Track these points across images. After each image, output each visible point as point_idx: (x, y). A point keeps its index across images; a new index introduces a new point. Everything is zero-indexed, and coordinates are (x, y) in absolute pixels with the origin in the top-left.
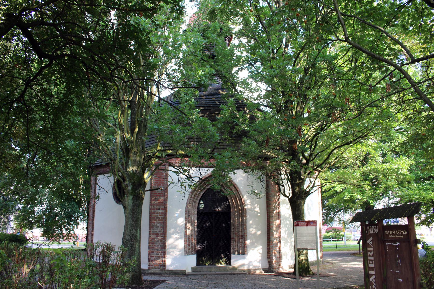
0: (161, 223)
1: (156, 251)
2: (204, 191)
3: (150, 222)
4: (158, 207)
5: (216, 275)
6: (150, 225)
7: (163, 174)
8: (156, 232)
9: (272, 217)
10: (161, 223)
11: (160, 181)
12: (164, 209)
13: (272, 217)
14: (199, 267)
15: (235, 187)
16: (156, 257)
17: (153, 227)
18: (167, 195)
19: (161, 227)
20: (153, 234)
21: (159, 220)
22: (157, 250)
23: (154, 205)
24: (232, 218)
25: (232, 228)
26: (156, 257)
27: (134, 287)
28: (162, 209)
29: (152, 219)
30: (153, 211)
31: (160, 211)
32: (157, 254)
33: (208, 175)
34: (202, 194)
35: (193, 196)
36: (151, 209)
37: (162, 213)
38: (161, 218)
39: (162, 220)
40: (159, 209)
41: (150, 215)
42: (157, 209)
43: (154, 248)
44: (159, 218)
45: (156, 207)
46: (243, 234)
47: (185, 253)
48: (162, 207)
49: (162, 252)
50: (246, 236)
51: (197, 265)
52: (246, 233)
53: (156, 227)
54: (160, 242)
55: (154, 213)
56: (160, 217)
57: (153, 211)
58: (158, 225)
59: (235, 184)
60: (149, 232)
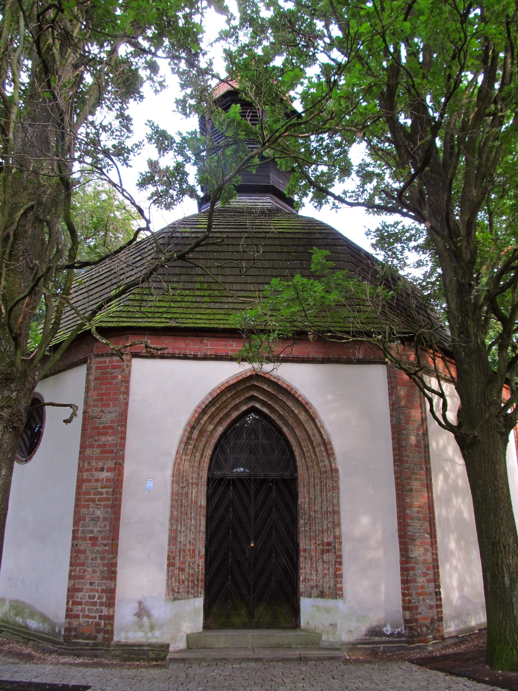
0: (105, 506)
1: (88, 586)
2: (225, 424)
3: (77, 506)
4: (100, 464)
5: (252, 664)
6: (76, 513)
7: (116, 377)
8: (92, 531)
9: (411, 490)
10: (105, 506)
11: (109, 394)
12: (114, 469)
13: (411, 490)
14: (210, 633)
15: (307, 411)
16: (87, 603)
17: (84, 519)
18: (124, 433)
19: (105, 519)
20: (84, 539)
21: (100, 500)
22: (91, 584)
23: (90, 458)
24: (300, 495)
25: (301, 522)
26: (87, 603)
27: (512, 580)
28: (109, 470)
29: (83, 497)
30: (85, 475)
31: (104, 475)
32: (90, 597)
33: (235, 380)
34: (220, 430)
35: (196, 433)
36: (81, 470)
37: (108, 480)
38: (107, 493)
39: (107, 499)
40: (102, 470)
41: (79, 487)
42: (96, 470)
43: (83, 577)
44: (101, 494)
45: (94, 464)
46: (331, 539)
47: (168, 594)
48: (110, 464)
49: (103, 591)
50: (340, 543)
51: (206, 627)
52: (340, 537)
53: (92, 519)
54: (99, 561)
55: (89, 481)
56: (104, 490)
57: (85, 475)
58: (98, 513)
59: (307, 403)
60: (74, 531)
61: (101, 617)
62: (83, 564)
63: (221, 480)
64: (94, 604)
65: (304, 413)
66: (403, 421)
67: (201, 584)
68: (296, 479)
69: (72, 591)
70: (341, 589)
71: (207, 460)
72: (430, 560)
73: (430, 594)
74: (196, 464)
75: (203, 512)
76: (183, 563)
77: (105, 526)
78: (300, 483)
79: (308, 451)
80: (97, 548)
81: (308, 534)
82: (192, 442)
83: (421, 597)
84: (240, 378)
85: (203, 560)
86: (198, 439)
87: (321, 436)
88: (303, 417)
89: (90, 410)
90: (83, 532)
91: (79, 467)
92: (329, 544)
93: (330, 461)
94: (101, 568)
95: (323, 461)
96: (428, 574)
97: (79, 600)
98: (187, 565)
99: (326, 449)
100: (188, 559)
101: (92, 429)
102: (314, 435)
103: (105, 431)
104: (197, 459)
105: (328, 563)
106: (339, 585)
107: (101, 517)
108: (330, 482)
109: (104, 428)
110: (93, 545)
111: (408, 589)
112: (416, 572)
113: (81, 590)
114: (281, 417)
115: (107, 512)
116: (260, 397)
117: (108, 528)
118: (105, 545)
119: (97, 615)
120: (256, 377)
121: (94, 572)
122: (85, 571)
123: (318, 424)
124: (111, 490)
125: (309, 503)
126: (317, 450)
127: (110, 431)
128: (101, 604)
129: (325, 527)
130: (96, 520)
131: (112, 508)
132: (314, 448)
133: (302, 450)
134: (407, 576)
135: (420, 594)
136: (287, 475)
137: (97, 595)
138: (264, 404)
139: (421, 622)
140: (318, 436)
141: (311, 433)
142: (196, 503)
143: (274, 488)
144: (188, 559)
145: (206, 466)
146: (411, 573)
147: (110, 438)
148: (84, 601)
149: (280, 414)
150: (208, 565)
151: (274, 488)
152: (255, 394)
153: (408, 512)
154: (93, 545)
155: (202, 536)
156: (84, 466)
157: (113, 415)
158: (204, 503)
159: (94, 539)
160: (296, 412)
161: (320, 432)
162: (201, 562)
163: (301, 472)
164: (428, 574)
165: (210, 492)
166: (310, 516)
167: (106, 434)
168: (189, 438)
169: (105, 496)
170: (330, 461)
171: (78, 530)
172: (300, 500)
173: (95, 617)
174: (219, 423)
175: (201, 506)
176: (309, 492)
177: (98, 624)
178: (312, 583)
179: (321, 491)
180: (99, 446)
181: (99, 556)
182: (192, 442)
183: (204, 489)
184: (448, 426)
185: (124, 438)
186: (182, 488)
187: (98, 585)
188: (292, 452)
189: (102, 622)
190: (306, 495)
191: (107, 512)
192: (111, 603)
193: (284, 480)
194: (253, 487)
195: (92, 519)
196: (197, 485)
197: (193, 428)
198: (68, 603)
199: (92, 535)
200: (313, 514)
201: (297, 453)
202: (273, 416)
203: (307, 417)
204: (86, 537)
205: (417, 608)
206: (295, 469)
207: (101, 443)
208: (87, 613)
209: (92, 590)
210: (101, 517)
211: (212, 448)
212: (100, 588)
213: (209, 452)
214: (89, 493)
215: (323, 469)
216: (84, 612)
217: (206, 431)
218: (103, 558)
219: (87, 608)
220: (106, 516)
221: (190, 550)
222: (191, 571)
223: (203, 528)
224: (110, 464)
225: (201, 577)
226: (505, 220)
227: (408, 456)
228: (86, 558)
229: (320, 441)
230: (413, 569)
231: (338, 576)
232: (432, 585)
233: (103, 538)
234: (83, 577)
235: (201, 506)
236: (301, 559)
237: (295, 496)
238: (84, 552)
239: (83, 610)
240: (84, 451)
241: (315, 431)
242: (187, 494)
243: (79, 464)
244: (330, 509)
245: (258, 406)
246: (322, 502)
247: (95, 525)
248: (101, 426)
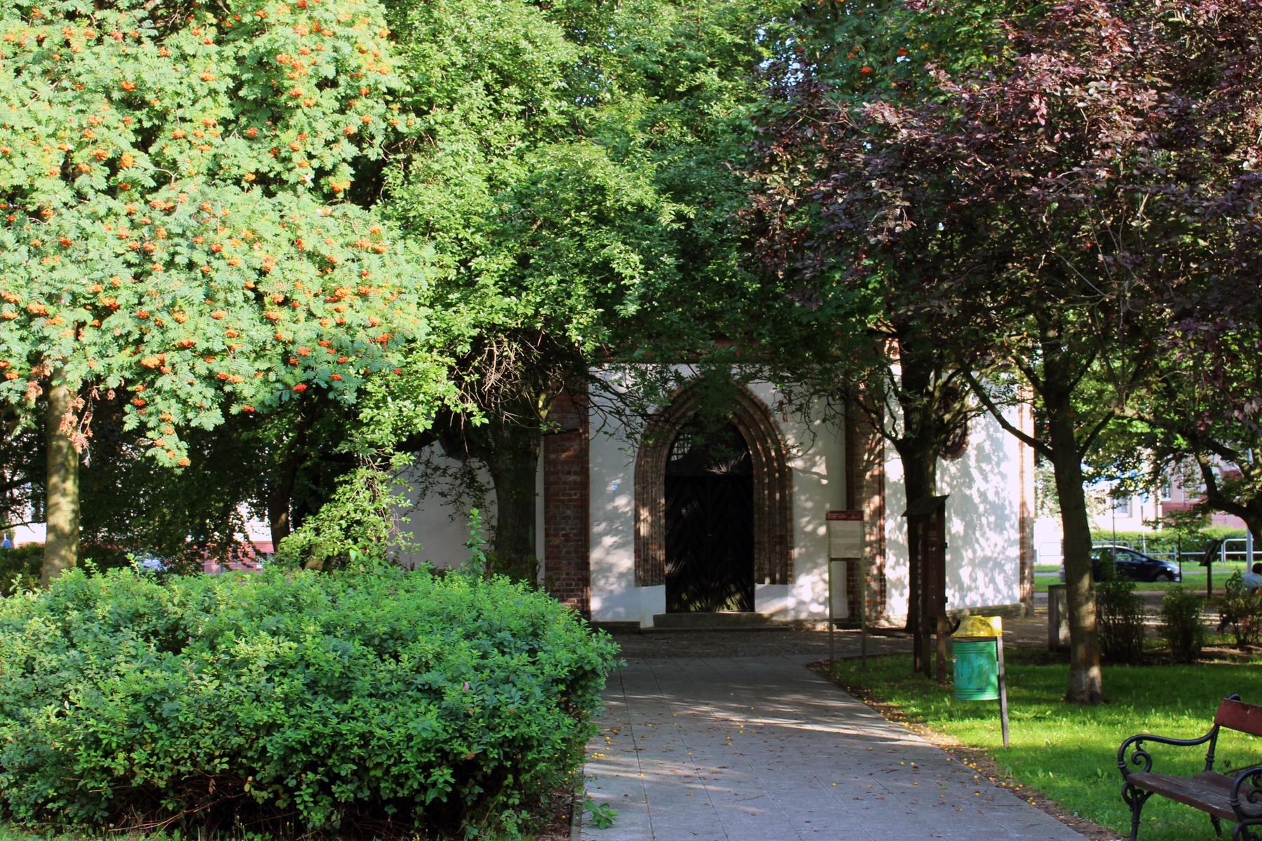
20: (556, 535)
28: (576, 473)
31: (572, 478)
37: (575, 482)
40: (569, 473)
53: (564, 518)
58: (569, 512)
88: (758, 416)
195: (564, 518)
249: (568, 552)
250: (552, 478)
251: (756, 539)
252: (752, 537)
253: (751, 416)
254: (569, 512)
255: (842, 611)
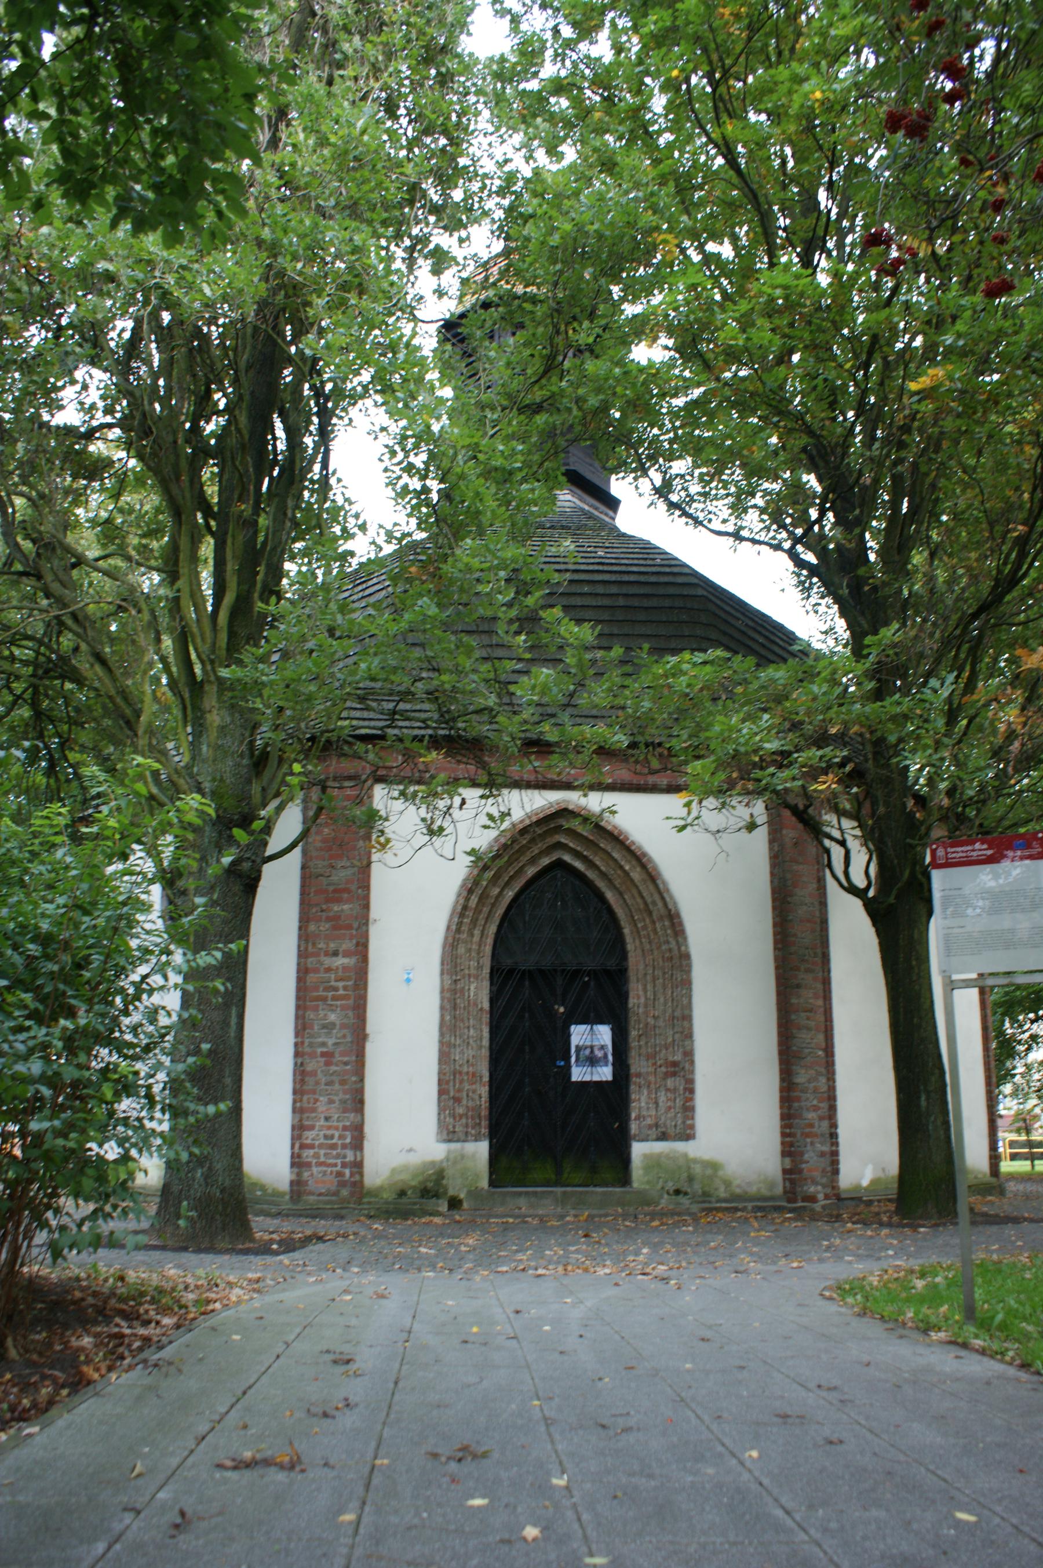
1: (322, 1122)
2: (517, 885)
8: (324, 1044)
10: (343, 1008)
15: (644, 866)
18: (366, 898)
19: (343, 1026)
20: (312, 1055)
21: (334, 998)
22: (327, 1119)
24: (631, 994)
25: (633, 1033)
26: (321, 1146)
28: (347, 954)
31: (340, 961)
34: (510, 894)
35: (474, 900)
37: (345, 968)
38: (345, 988)
40: (335, 954)
42: (327, 954)
44: (336, 989)
45: (322, 945)
46: (678, 1057)
53: (324, 1027)
54: (337, 1086)
55: (316, 971)
56: (340, 984)
58: (332, 1017)
59: (644, 854)
61: (344, 1165)
62: (314, 1092)
63: (511, 972)
64: (333, 1147)
65: (638, 869)
66: (789, 883)
67: (485, 1123)
68: (626, 970)
69: (298, 1130)
70: (692, 1127)
71: (490, 941)
72: (825, 1088)
73: (822, 1135)
74: (474, 947)
75: (486, 1018)
76: (459, 1091)
77: (344, 1036)
78: (632, 974)
79: (645, 928)
80: (333, 1068)
81: (643, 1051)
82: (470, 913)
83: (808, 1140)
84: (541, 816)
85: (487, 1088)
86: (477, 910)
87: (665, 904)
88: (636, 875)
89: (311, 864)
90: (311, 1045)
91: (299, 951)
92: (675, 1064)
93: (677, 942)
94: (341, 1096)
95: (668, 942)
96: (819, 1108)
97: (309, 1141)
98: (464, 1094)
99: (673, 925)
100: (467, 1086)
101: (316, 892)
102: (654, 903)
103: (337, 894)
104: (476, 939)
105: (674, 1090)
106: (689, 1122)
107: (338, 1023)
108: (679, 976)
109: (335, 891)
110: (328, 1064)
111: (790, 1126)
112: (803, 1104)
113: (312, 1128)
114: (603, 875)
115: (346, 1016)
116: (571, 845)
117: (349, 1039)
118: (346, 1064)
119: (339, 1161)
120: (564, 812)
121: (331, 1102)
122: (316, 1100)
123: (661, 886)
124: (350, 983)
125: (646, 1006)
126: (658, 925)
127: (346, 895)
128: (344, 1146)
129: (670, 1039)
130: (329, 1027)
131: (354, 1009)
132: (653, 922)
133: (636, 925)
134: (790, 1108)
135: (807, 1135)
136: (611, 964)
137: (337, 1134)
138: (577, 855)
139: (805, 1173)
140: (660, 904)
141: (649, 900)
142: (476, 1005)
143: (592, 983)
144: (467, 1086)
145: (488, 949)
146: (796, 1105)
147: (346, 907)
148: (317, 1143)
149: (601, 871)
150: (493, 1097)
151: (592, 983)
152: (563, 840)
153: (793, 1017)
154: (328, 1064)
155: (485, 1053)
156: (306, 949)
157: (349, 872)
158: (486, 1005)
159: (328, 1055)
160: (627, 868)
161: (663, 898)
162: (484, 1091)
163: (635, 962)
164: (819, 1108)
165: (495, 988)
166: (647, 1024)
167: (339, 901)
168: (465, 907)
169: (341, 992)
170: (677, 942)
171: (303, 1043)
172: (632, 1001)
173: (335, 1165)
174: (507, 884)
175: (481, 1009)
176: (645, 990)
177: (339, 1174)
178: (649, 1121)
179: (664, 987)
180: (329, 919)
181: (336, 1079)
182: (470, 913)
183: (486, 984)
184: (852, 889)
185: (367, 907)
186: (456, 981)
187: (338, 1121)
188: (619, 929)
189: (347, 1172)
190: (641, 993)
191: (346, 1016)
192: (358, 1143)
193: (607, 973)
194: (560, 980)
195: (324, 1027)
196: (476, 977)
197: (470, 891)
198: (293, 1146)
199: (325, 1050)
200: (651, 1021)
201: (626, 931)
202: (591, 874)
203: (645, 876)
204: (315, 1053)
205: (802, 1154)
206: (624, 955)
207: (331, 914)
208: (322, 1159)
209: (329, 1128)
210: (338, 1023)
211: (497, 923)
212: (341, 1124)
213: (492, 929)
214: (316, 989)
215: (667, 955)
216: (319, 1158)
217: (488, 896)
218: (343, 1082)
219: (322, 1152)
220: (345, 1021)
221: (467, 1073)
222: (470, 1104)
223: (486, 1042)
224: (348, 945)
225: (485, 1113)
226: (9, 1381)
227: (795, 935)
228: (317, 1083)
229: (663, 911)
230: (798, 1099)
231: (688, 1110)
232: (825, 1124)
233: (342, 1054)
234: (314, 1110)
235: (481, 1009)
236: (632, 1087)
237: (624, 997)
238: (314, 1073)
239: (316, 1156)
240: (307, 927)
241: (657, 897)
242: (462, 990)
243: (299, 946)
244: (677, 1014)
245: (567, 858)
246: (665, 1004)
247: (329, 1034)
248: (331, 888)
249: (329, 1083)
250: (311, 962)
251: (633, 1071)
252: (628, 1067)
253: (626, 874)
254: (332, 1017)
255: (843, 1196)
